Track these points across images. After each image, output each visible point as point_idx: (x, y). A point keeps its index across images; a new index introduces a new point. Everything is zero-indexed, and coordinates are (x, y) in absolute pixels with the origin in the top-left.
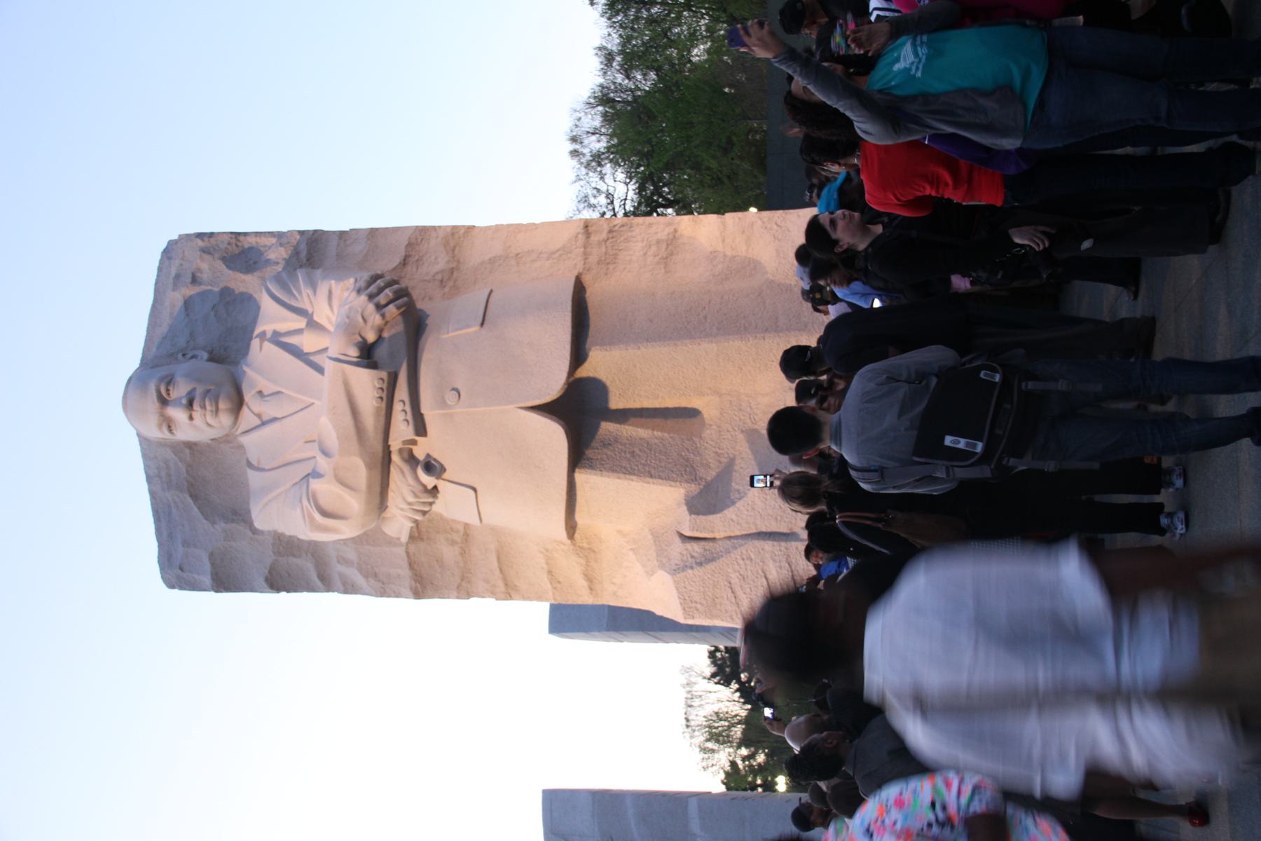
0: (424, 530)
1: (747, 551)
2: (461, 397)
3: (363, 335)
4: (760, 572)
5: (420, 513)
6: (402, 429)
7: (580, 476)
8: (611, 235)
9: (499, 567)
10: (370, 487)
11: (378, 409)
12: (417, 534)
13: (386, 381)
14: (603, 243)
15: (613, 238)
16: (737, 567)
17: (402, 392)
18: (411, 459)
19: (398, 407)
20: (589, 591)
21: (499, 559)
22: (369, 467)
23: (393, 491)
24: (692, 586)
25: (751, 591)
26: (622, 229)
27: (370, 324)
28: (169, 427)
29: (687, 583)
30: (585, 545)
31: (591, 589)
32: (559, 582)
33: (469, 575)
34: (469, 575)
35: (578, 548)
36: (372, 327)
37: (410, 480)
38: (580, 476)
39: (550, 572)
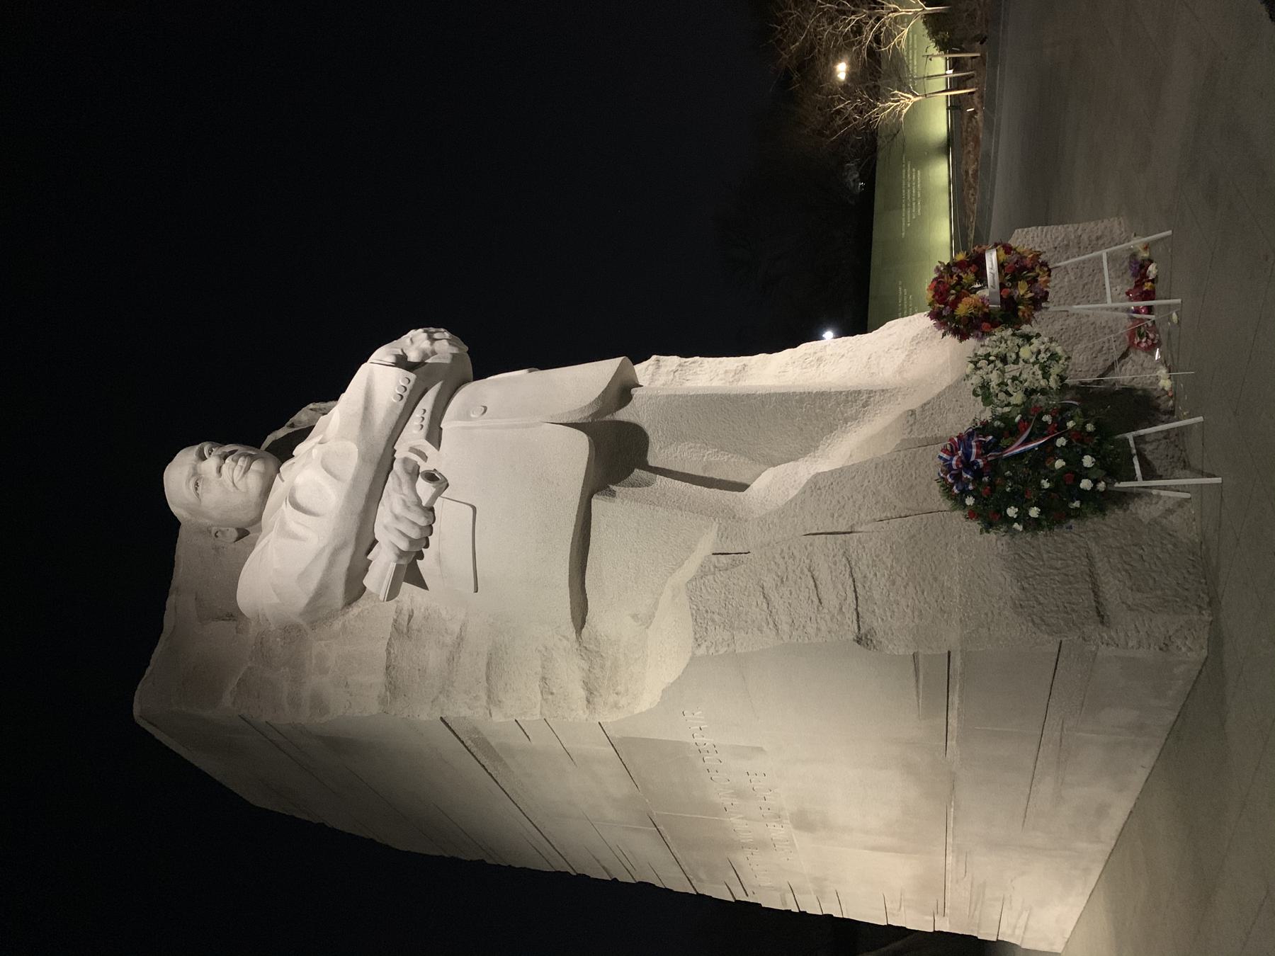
0: (415, 627)
1: (789, 548)
2: (530, 738)
3: (405, 351)
4: (806, 571)
5: (406, 539)
6: (414, 433)
7: (598, 504)
8: (680, 369)
9: (486, 673)
10: (356, 479)
11: (394, 406)
12: (405, 630)
13: (412, 383)
14: (672, 373)
15: (681, 370)
16: (773, 566)
17: (427, 402)
18: (414, 473)
19: (417, 414)
20: (586, 702)
21: (488, 664)
22: (363, 458)
23: (383, 505)
24: (709, 593)
25: (791, 594)
26: (693, 365)
27: (416, 345)
28: (197, 484)
29: (704, 591)
30: (591, 647)
31: (588, 701)
32: (552, 694)
33: (451, 688)
34: (451, 688)
35: (583, 649)
36: (417, 348)
37: (406, 489)
38: (598, 504)
39: (544, 679)
